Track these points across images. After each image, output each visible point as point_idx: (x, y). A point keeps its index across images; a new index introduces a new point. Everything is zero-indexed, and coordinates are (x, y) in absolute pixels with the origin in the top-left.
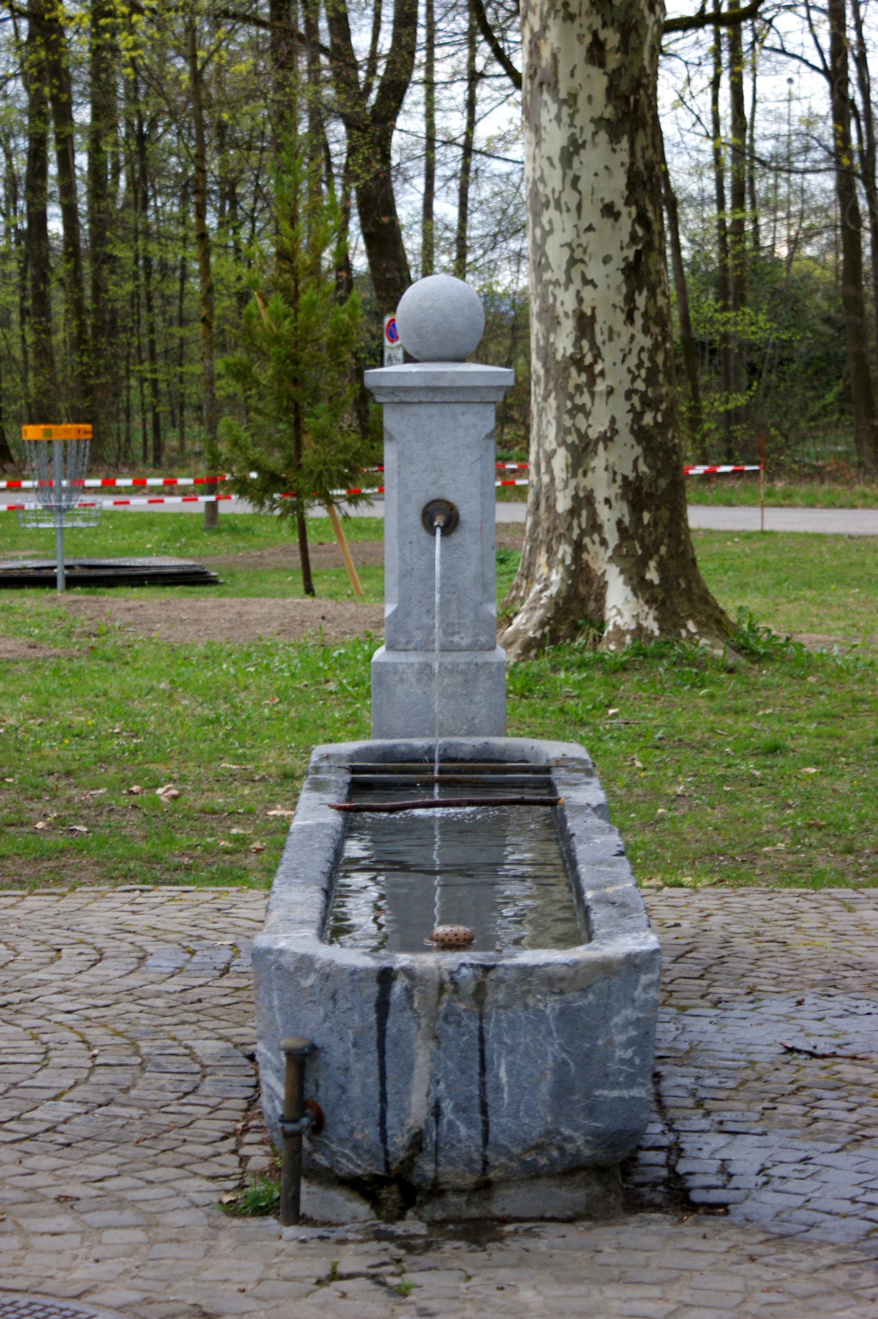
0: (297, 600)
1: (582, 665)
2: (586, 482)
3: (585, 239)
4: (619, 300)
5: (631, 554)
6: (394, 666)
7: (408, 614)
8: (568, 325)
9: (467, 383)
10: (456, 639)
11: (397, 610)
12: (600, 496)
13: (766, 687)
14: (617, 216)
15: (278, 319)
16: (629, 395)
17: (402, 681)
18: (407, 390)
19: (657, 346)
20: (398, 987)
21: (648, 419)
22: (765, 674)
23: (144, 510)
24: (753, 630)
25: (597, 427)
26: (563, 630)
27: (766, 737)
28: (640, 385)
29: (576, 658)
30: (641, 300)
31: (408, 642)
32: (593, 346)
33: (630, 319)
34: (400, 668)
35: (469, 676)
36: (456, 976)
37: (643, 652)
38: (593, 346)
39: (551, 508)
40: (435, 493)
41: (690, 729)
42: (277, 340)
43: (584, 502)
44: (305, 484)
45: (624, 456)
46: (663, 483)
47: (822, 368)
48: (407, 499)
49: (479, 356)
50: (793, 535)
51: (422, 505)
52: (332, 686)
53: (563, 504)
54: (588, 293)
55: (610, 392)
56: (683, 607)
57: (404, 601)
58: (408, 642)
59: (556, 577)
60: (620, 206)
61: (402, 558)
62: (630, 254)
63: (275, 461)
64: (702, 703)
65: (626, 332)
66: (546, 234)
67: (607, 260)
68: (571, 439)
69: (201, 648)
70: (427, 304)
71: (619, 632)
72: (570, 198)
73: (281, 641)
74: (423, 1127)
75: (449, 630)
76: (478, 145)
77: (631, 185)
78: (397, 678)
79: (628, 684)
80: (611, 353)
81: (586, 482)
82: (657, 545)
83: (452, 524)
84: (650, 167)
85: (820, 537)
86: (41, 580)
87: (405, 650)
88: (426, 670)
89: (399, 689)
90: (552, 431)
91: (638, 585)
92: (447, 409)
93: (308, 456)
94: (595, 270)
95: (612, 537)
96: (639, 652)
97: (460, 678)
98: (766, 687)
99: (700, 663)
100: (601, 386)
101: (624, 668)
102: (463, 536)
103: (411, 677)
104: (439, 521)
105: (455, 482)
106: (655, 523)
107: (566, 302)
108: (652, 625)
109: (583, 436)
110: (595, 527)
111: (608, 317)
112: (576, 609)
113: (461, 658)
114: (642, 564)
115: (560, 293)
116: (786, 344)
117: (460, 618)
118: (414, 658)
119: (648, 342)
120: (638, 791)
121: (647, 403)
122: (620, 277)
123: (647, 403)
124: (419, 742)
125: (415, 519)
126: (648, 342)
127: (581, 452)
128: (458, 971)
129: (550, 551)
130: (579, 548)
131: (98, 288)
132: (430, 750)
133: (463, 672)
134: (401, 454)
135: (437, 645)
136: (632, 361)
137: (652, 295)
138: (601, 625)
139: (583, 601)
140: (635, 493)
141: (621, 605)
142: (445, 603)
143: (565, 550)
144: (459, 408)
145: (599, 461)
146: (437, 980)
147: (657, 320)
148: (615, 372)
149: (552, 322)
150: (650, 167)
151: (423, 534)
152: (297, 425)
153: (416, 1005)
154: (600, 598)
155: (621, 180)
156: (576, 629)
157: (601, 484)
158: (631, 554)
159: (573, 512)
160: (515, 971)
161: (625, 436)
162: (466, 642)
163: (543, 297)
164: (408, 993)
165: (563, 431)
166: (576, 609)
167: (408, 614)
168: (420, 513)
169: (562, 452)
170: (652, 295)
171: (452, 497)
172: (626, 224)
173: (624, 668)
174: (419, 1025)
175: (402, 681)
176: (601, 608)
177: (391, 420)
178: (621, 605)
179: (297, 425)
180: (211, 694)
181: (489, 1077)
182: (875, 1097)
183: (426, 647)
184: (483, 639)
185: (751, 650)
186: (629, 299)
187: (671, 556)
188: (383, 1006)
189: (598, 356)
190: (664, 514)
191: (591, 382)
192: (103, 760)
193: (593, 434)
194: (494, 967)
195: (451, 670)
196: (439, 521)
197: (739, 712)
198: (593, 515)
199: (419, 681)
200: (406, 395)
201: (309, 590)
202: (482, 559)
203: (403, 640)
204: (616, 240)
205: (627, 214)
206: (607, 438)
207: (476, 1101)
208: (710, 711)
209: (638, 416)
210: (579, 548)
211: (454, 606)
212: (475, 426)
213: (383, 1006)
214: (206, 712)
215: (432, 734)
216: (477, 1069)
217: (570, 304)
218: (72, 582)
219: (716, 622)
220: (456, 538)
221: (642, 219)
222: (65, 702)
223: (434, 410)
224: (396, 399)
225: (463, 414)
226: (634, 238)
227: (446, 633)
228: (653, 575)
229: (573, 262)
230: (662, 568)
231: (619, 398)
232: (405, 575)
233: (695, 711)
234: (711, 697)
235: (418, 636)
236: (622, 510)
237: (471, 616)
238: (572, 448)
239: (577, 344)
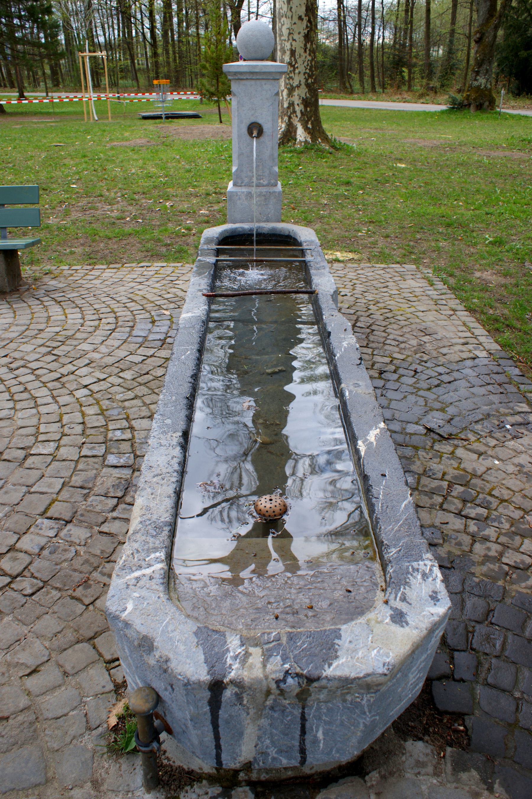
0: (218, 125)
1: (291, 151)
2: (292, 99)
3: (293, 27)
4: (303, 46)
5: (304, 120)
6: (236, 192)
7: (242, 171)
8: (288, 53)
12: (296, 103)
13: (341, 159)
14: (302, 20)
15: (213, 52)
16: (304, 74)
17: (239, 199)
18: (241, 73)
19: (313, 59)
20: (228, 694)
21: (310, 81)
22: (340, 155)
23: (186, 99)
24: (335, 140)
25: (296, 83)
26: (285, 141)
27: (344, 179)
28: (308, 71)
29: (289, 149)
30: (308, 46)
32: (295, 59)
33: (305, 51)
35: (266, 197)
36: (282, 685)
37: (307, 148)
38: (295, 59)
39: (282, 106)
40: (253, 120)
41: (323, 174)
42: (212, 58)
43: (291, 104)
44: (220, 95)
45: (303, 92)
46: (313, 99)
47: (331, 68)
48: (241, 122)
50: (329, 106)
52: (223, 157)
53: (286, 105)
54: (294, 43)
55: (299, 73)
56: (317, 135)
57: (240, 166)
59: (283, 126)
60: (303, 17)
61: (240, 148)
62: (306, 31)
63: (213, 89)
64: (325, 164)
65: (304, 55)
66: (283, 25)
67: (299, 33)
68: (288, 86)
69: (191, 142)
70: (250, 33)
71: (301, 142)
72: (289, 14)
73: (213, 139)
74: (252, 760)
75: (259, 178)
76: (260, 13)
77: (306, 10)
79: (303, 158)
80: (300, 61)
81: (292, 99)
82: (311, 117)
83: (260, 132)
84: (312, 5)
85: (335, 107)
86: (159, 117)
88: (249, 195)
89: (238, 202)
90: (283, 84)
91: (306, 129)
92: (258, 82)
93: (220, 88)
94: (296, 37)
95: (299, 115)
96: (306, 148)
98: (341, 159)
99: (322, 151)
100: (297, 71)
101: (302, 152)
102: (264, 138)
103: (243, 197)
104: (255, 134)
106: (311, 111)
107: (288, 46)
108: (309, 140)
109: (291, 86)
110: (294, 112)
111: (299, 51)
112: (289, 136)
113: (264, 190)
114: (307, 123)
115: (286, 43)
116: (324, 62)
118: (245, 190)
119: (310, 58)
120: (312, 202)
121: (310, 76)
122: (303, 39)
123: (310, 76)
124: (246, 226)
125: (245, 130)
126: (310, 58)
127: (291, 90)
128: (284, 681)
129: (282, 119)
130: (290, 118)
131: (179, 48)
132: (251, 230)
134: (238, 102)
135: (254, 184)
136: (306, 64)
137: (312, 44)
138: (296, 140)
139: (291, 133)
140: (306, 102)
141: (301, 134)
142: (257, 166)
143: (286, 118)
144: (263, 82)
145: (296, 93)
146: (265, 689)
147: (313, 52)
148: (301, 67)
149: (284, 52)
150: (312, 5)
151: (248, 137)
152: (217, 80)
153: (245, 702)
154: (295, 132)
155: (304, 8)
156: (289, 141)
157: (297, 100)
158: (304, 120)
159: (288, 108)
160: (336, 682)
161: (303, 86)
162: (265, 183)
163: (281, 45)
164: (239, 697)
165: (286, 84)
166: (289, 136)
167: (242, 171)
169: (286, 90)
170: (312, 44)
171: (260, 121)
172: (305, 22)
173: (302, 152)
174: (248, 714)
175: (239, 199)
176: (295, 135)
177: (234, 87)
178: (301, 134)
179: (217, 80)
180: (191, 160)
181: (308, 738)
183: (249, 185)
184: (272, 181)
185: (336, 147)
186: (305, 45)
187: (315, 120)
188: (215, 703)
189: (296, 62)
190: (313, 108)
191: (294, 70)
192: (155, 187)
193: (294, 85)
194: (318, 679)
195: (260, 195)
196: (255, 134)
197: (335, 167)
198: (294, 109)
199: (246, 199)
200: (241, 76)
201: (221, 122)
202: (272, 148)
203: (240, 182)
204: (302, 27)
205: (306, 19)
206: (298, 86)
207: (297, 748)
208: (327, 167)
209: (307, 80)
210: (290, 118)
213: (215, 703)
214: (187, 167)
215: (252, 222)
216: (299, 733)
217: (289, 47)
218: (167, 118)
219: (326, 139)
220: (262, 139)
221: (309, 21)
222: (151, 163)
223: (253, 82)
226: (307, 27)
227: (257, 179)
228: (310, 126)
229: (290, 34)
230: (312, 124)
231: (302, 75)
232: (240, 155)
233: (321, 167)
234: (326, 162)
235: (246, 180)
236: (302, 107)
237: (268, 172)
238: (288, 89)
239: (290, 59)
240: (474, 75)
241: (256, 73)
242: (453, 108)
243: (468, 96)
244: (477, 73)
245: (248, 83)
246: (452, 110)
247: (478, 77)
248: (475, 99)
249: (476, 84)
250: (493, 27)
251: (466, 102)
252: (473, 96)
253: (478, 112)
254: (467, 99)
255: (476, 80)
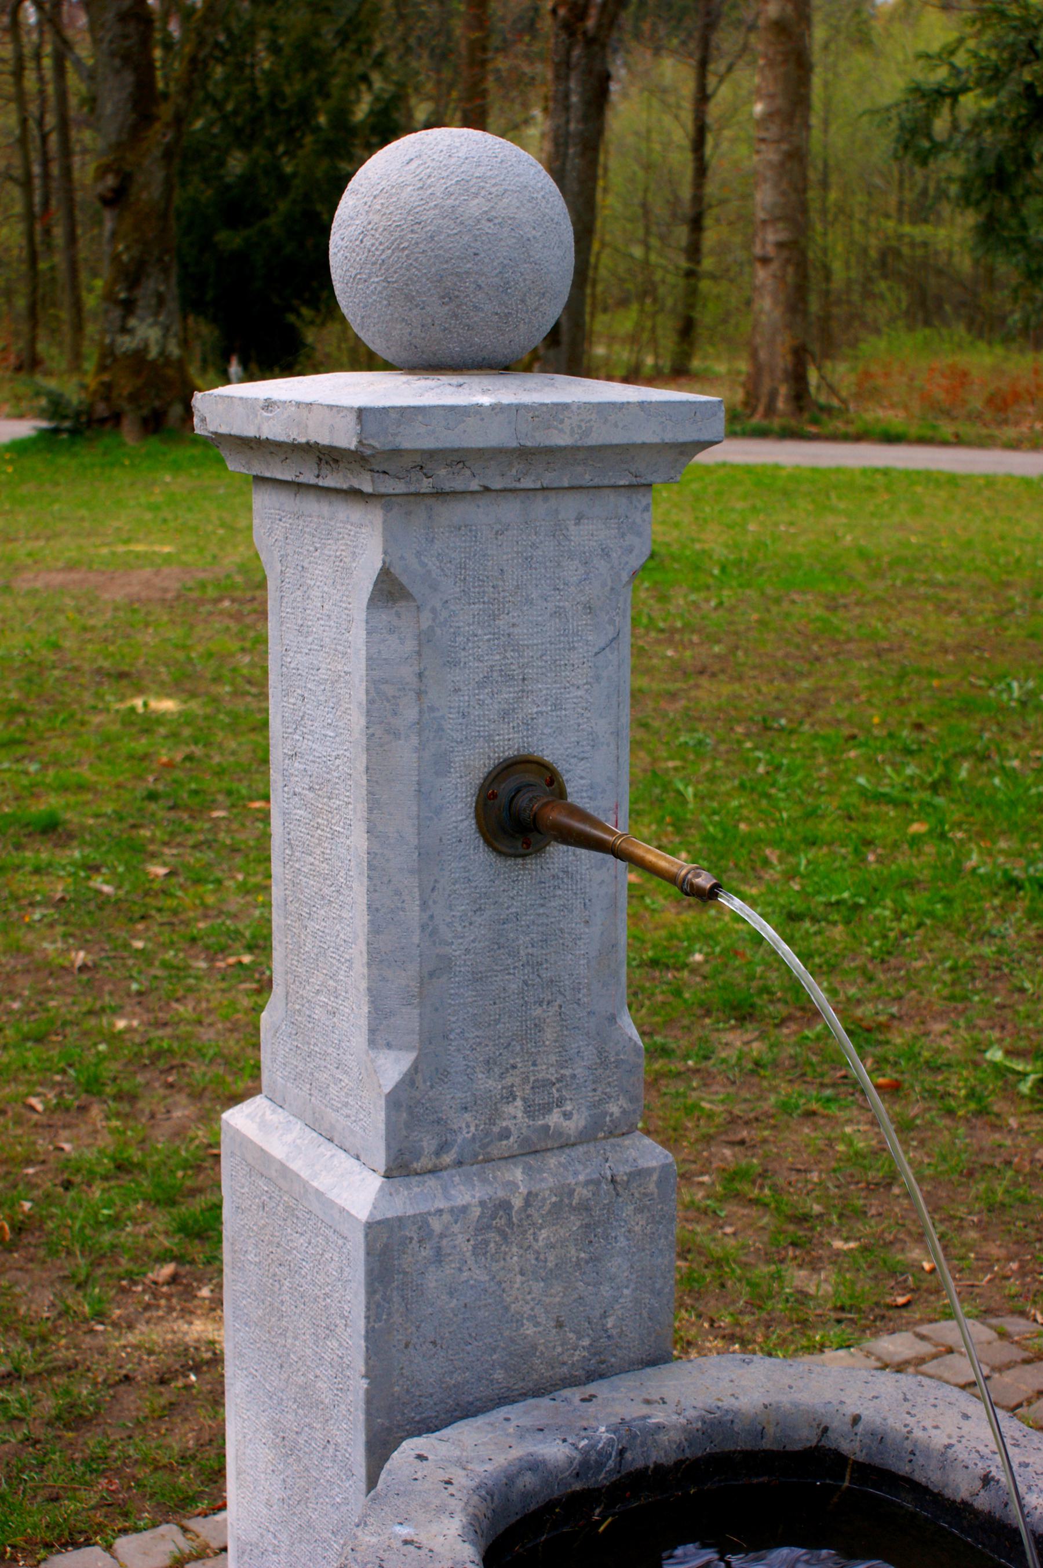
6: (421, 1221)
7: (442, 1075)
9: (561, 439)
10: (554, 1119)
11: (415, 1068)
18: (459, 458)
31: (443, 1148)
34: (436, 1225)
40: (509, 743)
48: (442, 764)
49: (564, 349)
51: (477, 777)
58: (443, 1148)
70: (475, 207)
78: (427, 1252)
87: (433, 1171)
88: (499, 1221)
89: (432, 1280)
92: (540, 507)
97: (575, 1223)
105: (557, 707)
117: (561, 1065)
118: (467, 1194)
133: (584, 1207)
144: (569, 505)
167: (442, 1075)
168: (472, 800)
171: (550, 751)
182: (4, 1442)
199: (480, 1249)
203: (428, 1144)
211: (549, 1035)
212: (606, 553)
223: (509, 510)
224: (426, 485)
225: (579, 519)
235: (466, 1127)
237: (589, 1053)
240: (116, 313)
241: (550, 452)
242: (56, 431)
243: (108, 386)
244: (128, 307)
245: (481, 515)
246: (47, 441)
247: (132, 322)
248: (133, 398)
249: (126, 343)
250: (157, 152)
251: (101, 409)
252: (126, 385)
253: (154, 443)
254: (107, 399)
255: (124, 330)
